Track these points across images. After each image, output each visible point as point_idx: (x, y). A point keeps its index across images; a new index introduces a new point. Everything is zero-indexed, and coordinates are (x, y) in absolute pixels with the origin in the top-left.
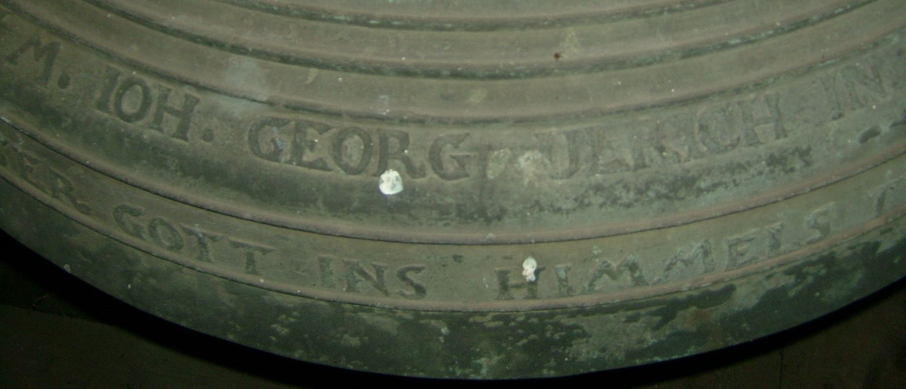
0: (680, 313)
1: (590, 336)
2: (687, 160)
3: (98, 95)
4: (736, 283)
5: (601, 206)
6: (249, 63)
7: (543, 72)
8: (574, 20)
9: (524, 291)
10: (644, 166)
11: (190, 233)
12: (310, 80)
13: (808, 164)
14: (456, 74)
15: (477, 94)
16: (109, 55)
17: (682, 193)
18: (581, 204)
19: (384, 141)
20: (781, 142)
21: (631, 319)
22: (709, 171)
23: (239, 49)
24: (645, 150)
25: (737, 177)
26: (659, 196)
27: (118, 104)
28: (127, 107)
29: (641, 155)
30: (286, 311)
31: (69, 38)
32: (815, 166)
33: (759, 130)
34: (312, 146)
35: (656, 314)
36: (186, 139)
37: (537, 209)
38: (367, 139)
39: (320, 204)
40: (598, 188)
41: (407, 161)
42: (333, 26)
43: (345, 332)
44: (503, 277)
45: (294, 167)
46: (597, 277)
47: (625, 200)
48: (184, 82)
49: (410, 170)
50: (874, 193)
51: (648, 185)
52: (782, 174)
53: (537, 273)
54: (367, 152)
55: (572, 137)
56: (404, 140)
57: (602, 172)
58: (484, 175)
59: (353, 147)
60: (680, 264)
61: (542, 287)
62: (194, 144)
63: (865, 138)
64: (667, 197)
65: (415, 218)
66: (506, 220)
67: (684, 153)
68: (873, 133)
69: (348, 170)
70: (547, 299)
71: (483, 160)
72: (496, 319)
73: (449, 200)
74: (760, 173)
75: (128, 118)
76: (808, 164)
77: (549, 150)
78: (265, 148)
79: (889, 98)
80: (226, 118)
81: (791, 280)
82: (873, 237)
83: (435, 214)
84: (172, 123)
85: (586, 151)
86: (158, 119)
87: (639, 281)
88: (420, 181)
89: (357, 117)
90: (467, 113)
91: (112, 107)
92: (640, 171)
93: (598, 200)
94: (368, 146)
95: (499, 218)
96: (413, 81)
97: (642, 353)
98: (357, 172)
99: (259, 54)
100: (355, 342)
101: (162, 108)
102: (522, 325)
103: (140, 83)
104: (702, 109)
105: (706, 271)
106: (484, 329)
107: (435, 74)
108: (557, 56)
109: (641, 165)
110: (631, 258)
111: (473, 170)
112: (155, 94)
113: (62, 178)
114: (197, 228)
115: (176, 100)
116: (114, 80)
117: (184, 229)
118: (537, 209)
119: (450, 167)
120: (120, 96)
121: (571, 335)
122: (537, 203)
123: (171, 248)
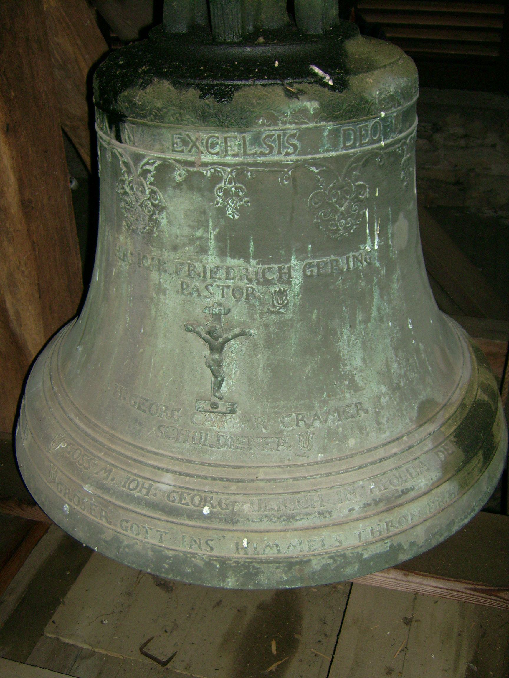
0: (294, 568)
1: (264, 573)
2: (293, 510)
3: (123, 483)
4: (312, 558)
5: (267, 521)
6: (169, 475)
7: (252, 481)
8: (261, 467)
9: (243, 551)
10: (280, 511)
11: (144, 527)
12: (187, 480)
13: (331, 516)
14: (228, 480)
15: (233, 488)
16: (128, 472)
17: (291, 520)
18: (261, 520)
19: (206, 498)
20: (322, 508)
21: (278, 568)
22: (300, 514)
23: (167, 471)
24: (281, 506)
25: (308, 517)
26: (284, 520)
27: (129, 486)
28: (131, 487)
29: (280, 508)
30: (168, 557)
31: (116, 467)
32: (333, 517)
33: (316, 504)
34: (185, 499)
35: (285, 566)
36: (148, 496)
37: (248, 521)
38: (201, 497)
39: (185, 516)
40: (266, 516)
41: (212, 504)
42: (195, 465)
43: (187, 566)
44: (237, 544)
45: (179, 505)
46: (266, 548)
47: (274, 520)
48: (150, 480)
49: (213, 507)
50: (357, 532)
51: (281, 516)
52: (323, 518)
53: (247, 544)
54: (201, 501)
55: (260, 501)
56: (212, 498)
57: (267, 511)
58: (233, 510)
59: (197, 500)
60: (292, 547)
61: (249, 550)
62: (150, 497)
63: (350, 511)
64: (287, 521)
65: (212, 521)
66: (239, 524)
67: (292, 508)
68: (353, 509)
69: (195, 506)
70: (251, 554)
71: (233, 506)
72: (235, 562)
73: (223, 516)
74: (316, 517)
75: (131, 490)
76: (331, 516)
77: (252, 504)
78: (171, 499)
79: (358, 500)
80: (161, 490)
81: (331, 561)
82: (360, 550)
83: (218, 520)
84: (144, 491)
85: (263, 505)
86: (140, 490)
87: (279, 551)
88: (215, 510)
89: (198, 491)
90: (230, 492)
91: (127, 487)
92: (279, 512)
93: (266, 519)
94: (201, 500)
95: (237, 523)
96: (216, 482)
97: (282, 583)
98: (197, 507)
99: (173, 472)
100: (189, 570)
101: (142, 487)
102: (243, 565)
103: (136, 480)
104: (298, 496)
105: (301, 551)
106: (231, 567)
107: (221, 480)
108: (257, 477)
109: (279, 510)
110: (276, 542)
111: (231, 508)
112: (141, 483)
113: (105, 511)
114: (146, 526)
115: (147, 485)
116: (128, 479)
117: (142, 526)
118: (248, 521)
119: (224, 506)
120: (130, 484)
121: (258, 572)
122: (248, 519)
123: (136, 535)
